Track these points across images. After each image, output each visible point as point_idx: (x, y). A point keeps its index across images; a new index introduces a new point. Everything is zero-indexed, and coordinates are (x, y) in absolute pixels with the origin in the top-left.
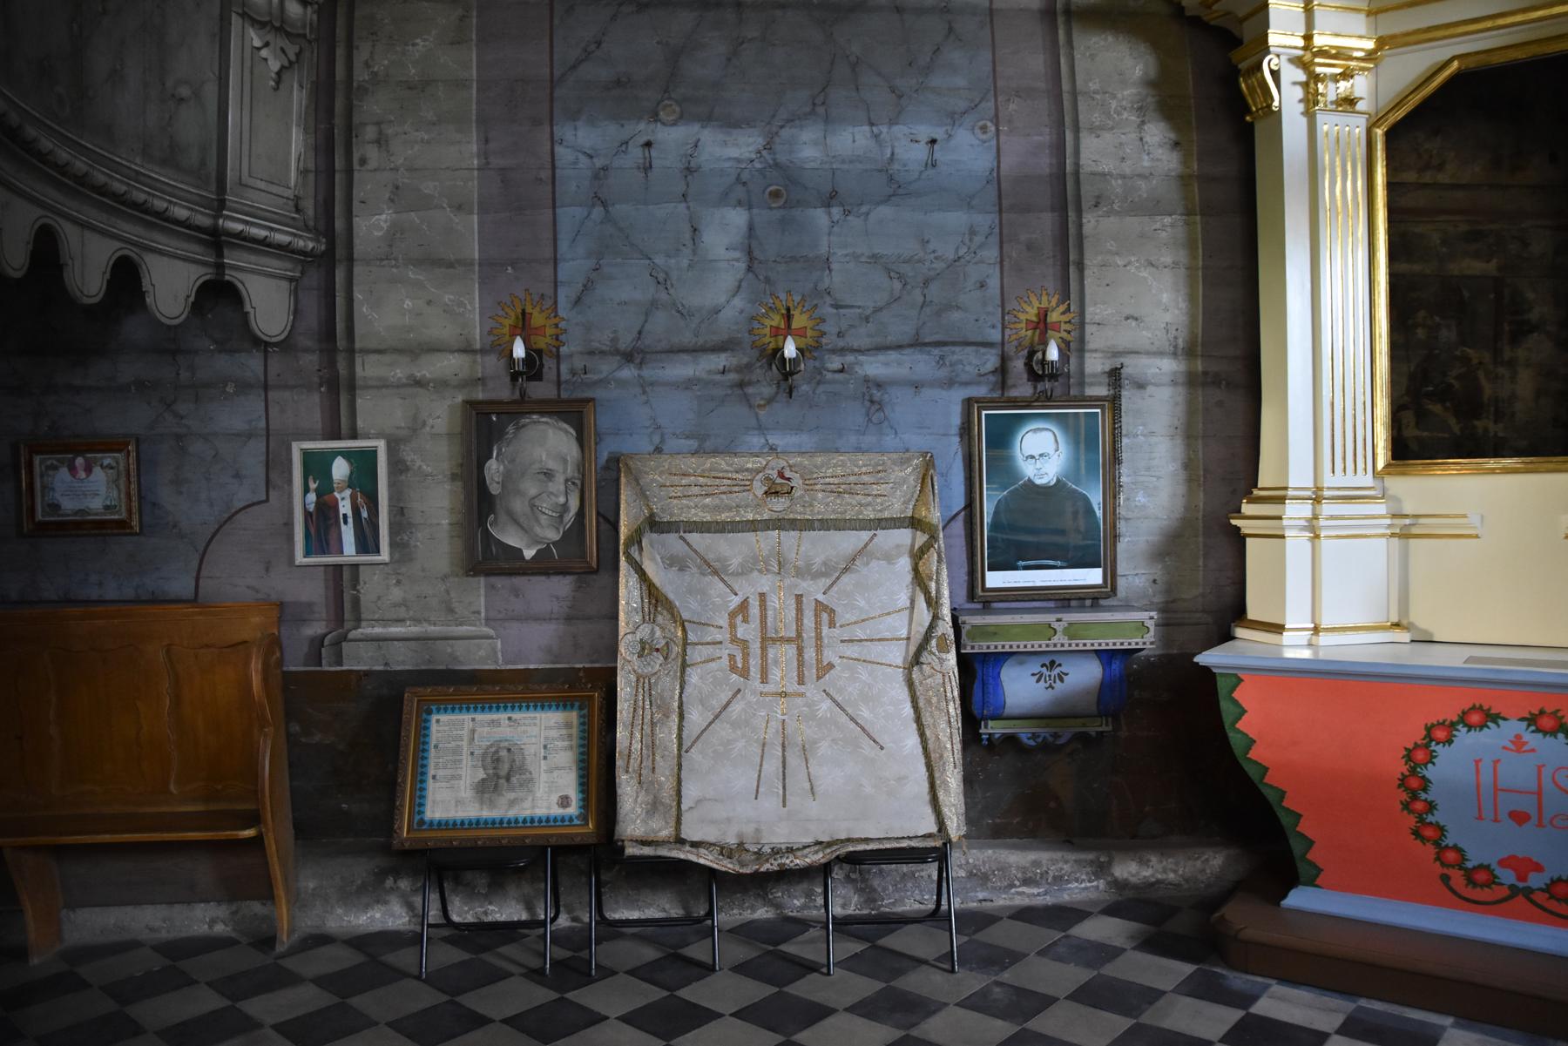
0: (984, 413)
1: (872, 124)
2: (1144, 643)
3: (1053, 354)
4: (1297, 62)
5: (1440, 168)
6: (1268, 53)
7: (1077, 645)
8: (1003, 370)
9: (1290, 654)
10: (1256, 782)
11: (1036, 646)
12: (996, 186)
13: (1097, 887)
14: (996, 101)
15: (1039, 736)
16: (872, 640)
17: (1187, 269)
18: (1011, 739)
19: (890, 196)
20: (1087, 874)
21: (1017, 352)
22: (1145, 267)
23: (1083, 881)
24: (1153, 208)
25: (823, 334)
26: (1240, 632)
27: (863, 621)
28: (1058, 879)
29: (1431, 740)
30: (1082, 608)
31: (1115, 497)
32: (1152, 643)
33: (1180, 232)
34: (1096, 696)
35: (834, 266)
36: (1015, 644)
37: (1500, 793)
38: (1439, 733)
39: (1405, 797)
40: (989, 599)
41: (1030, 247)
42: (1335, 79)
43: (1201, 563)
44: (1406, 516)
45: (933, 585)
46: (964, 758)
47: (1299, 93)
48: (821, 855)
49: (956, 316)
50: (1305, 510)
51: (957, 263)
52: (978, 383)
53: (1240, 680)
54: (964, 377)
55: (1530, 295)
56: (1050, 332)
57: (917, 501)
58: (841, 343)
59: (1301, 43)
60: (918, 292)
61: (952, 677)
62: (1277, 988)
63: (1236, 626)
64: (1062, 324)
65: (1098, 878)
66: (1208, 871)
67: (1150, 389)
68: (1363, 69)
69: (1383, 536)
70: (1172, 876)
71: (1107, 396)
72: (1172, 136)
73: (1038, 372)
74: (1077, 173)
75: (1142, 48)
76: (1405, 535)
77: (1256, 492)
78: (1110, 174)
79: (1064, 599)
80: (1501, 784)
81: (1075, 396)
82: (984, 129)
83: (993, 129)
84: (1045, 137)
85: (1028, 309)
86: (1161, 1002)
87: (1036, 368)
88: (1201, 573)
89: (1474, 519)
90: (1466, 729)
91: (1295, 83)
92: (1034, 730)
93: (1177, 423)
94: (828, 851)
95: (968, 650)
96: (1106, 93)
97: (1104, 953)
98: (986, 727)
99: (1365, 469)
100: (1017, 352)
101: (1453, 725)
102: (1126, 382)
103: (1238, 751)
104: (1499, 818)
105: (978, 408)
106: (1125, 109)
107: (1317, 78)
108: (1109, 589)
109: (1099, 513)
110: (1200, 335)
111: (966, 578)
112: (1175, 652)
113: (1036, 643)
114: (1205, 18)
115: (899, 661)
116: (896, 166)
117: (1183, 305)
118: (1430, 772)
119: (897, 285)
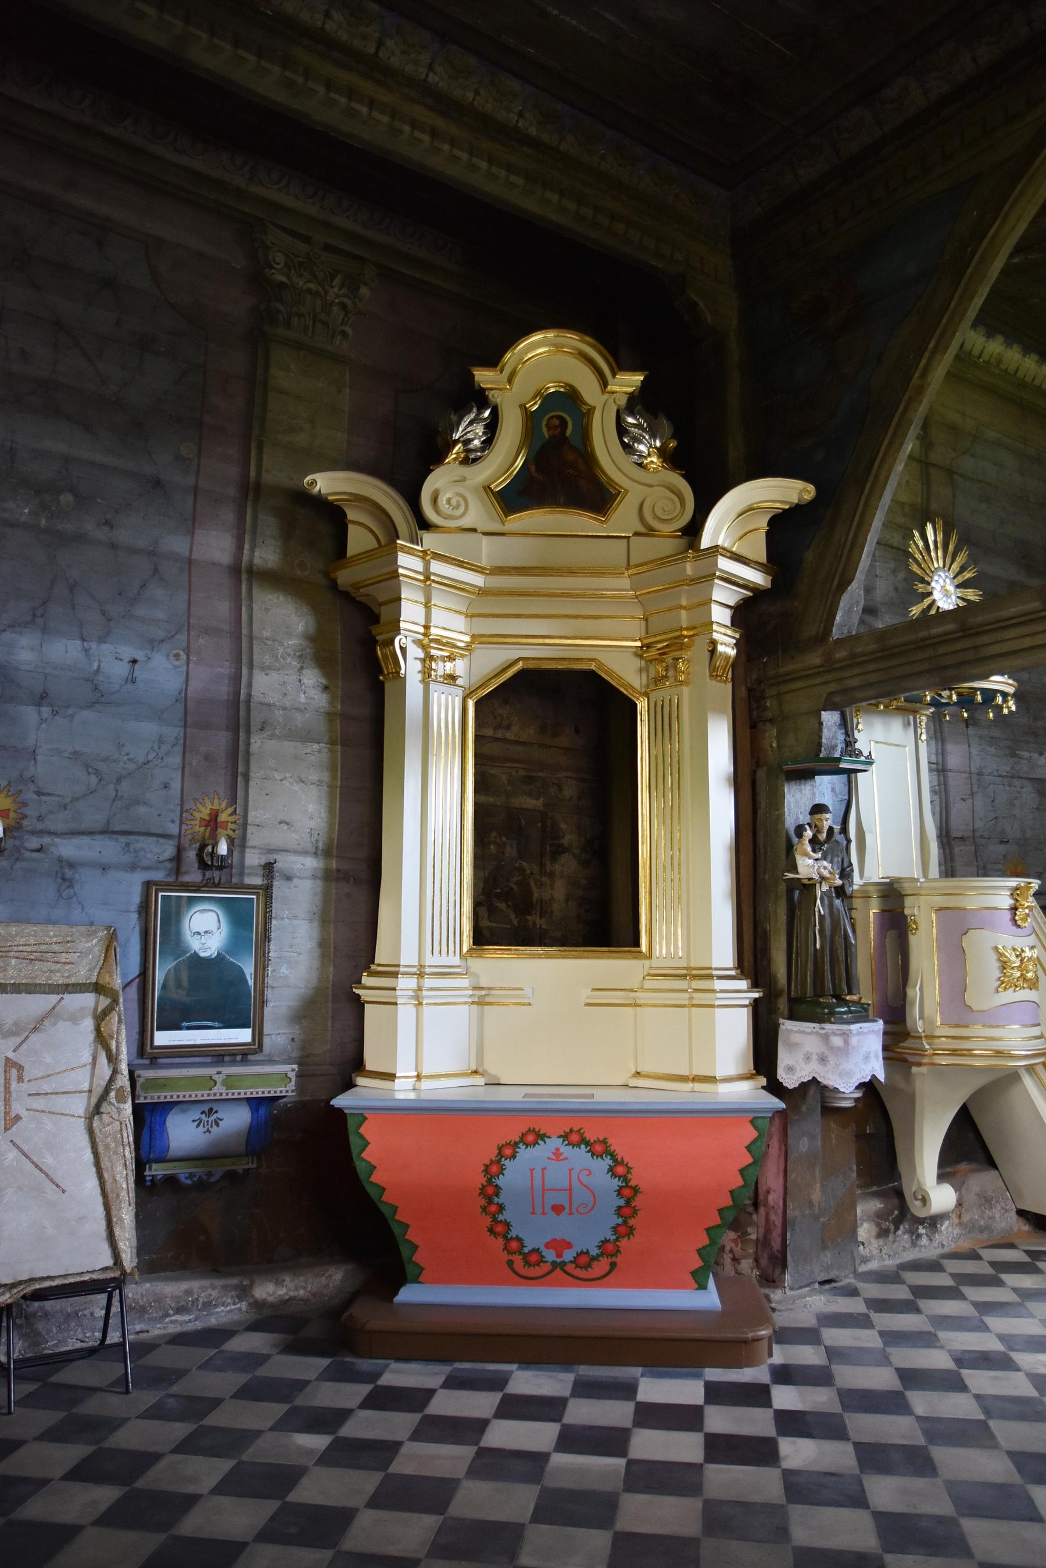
0: (160, 894)
1: (83, 640)
2: (287, 1092)
3: (223, 849)
4: (418, 643)
6: (400, 634)
7: (233, 1094)
8: (178, 858)
9: (400, 1096)
10: (376, 1201)
11: (199, 1096)
12: (183, 705)
13: (240, 1309)
14: (189, 635)
15: (195, 1176)
16: (57, 1093)
17: (328, 787)
18: (171, 1180)
19: (94, 703)
20: (232, 1297)
21: (191, 844)
22: (297, 783)
23: (228, 1304)
24: (305, 737)
25: (24, 817)
26: (361, 1081)
27: (48, 1076)
28: (208, 1305)
29: (502, 1157)
30: (233, 1063)
31: (264, 969)
32: (293, 1091)
33: (325, 756)
34: (245, 1138)
35: (39, 758)
36: (181, 1094)
37: (547, 1194)
39: (483, 1202)
40: (155, 1055)
41: (207, 758)
42: (444, 659)
43: (330, 1025)
44: (482, 988)
45: (113, 1044)
46: (137, 1197)
47: (418, 666)
48: (8, 1295)
49: (142, 810)
50: (411, 983)
51: (146, 766)
52: (157, 869)
53: (365, 1119)
54: (145, 863)
55: (563, 826)
56: (219, 830)
57: (101, 968)
58: (40, 826)
59: (422, 630)
60: (111, 787)
61: (128, 1125)
62: (394, 1365)
63: (357, 1076)
64: (229, 823)
65: (241, 1300)
66: (331, 1285)
67: (295, 881)
68: (462, 656)
69: (466, 1003)
70: (302, 1292)
71: (262, 885)
72: (324, 681)
73: (207, 862)
74: (248, 702)
75: (305, 609)
76: (481, 1003)
77: (373, 967)
78: (274, 705)
79: (220, 1055)
80: (547, 1185)
81: (236, 884)
82: (177, 656)
83: (184, 657)
84: (225, 669)
85: (202, 809)
86: (308, 1389)
87: (206, 859)
88: (330, 1032)
89: (528, 992)
90: (524, 1146)
91: (416, 658)
92: (192, 1170)
93: (316, 910)
94: (15, 1291)
95: (141, 1101)
96: (275, 640)
97: (252, 1360)
98: (150, 1169)
99: (455, 952)
100: (191, 844)
101: (516, 1144)
103: (362, 1175)
104: (545, 1212)
105: (156, 890)
107: (432, 658)
108: (257, 1047)
109: (251, 982)
111: (137, 1037)
112: (307, 1098)
113: (199, 1093)
114: (353, 595)
115: (81, 1112)
116: (101, 678)
117: (324, 815)
118: (501, 1181)
119: (94, 780)
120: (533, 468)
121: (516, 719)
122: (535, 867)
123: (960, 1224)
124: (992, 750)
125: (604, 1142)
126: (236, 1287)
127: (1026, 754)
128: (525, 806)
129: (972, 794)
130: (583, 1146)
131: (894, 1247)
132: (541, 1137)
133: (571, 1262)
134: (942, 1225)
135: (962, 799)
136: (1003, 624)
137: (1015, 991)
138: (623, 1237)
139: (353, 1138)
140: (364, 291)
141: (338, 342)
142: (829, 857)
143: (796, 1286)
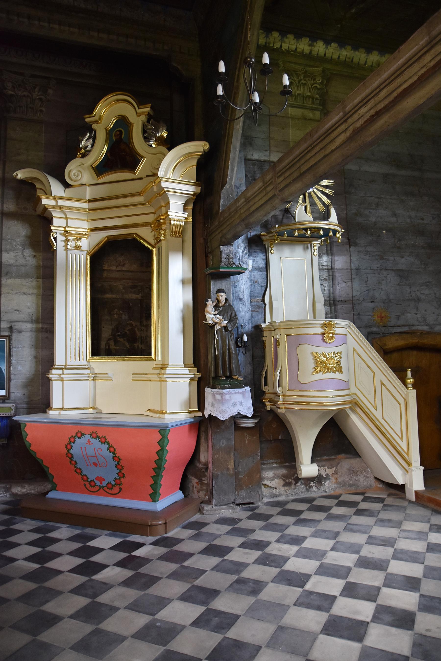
5: (123, 265)
13: (6, 496)
20: (2, 491)
24: (26, 276)
38: (72, 440)
39: (69, 460)
43: (40, 389)
47: (63, 244)
65: (6, 493)
66: (46, 489)
67: (23, 333)
70: (33, 491)
78: (12, 265)
89: (110, 375)
91: (62, 241)
93: (33, 344)
101: (75, 437)
102: (15, 331)
106: (18, 245)
107: (69, 240)
110: (40, 316)
120: (109, 154)
121: (127, 261)
122: (138, 323)
123: (337, 483)
124: (367, 257)
125: (104, 437)
126: (4, 488)
127: (391, 258)
128: (131, 298)
129: (352, 279)
130: (97, 439)
131: (295, 491)
132: (83, 434)
133: (105, 486)
134: (325, 482)
135: (344, 282)
136: (255, 194)
137: (323, 374)
138: (122, 478)
139: (23, 433)
140: (50, 91)
141: (38, 115)
142: (222, 313)
143: (219, 505)
